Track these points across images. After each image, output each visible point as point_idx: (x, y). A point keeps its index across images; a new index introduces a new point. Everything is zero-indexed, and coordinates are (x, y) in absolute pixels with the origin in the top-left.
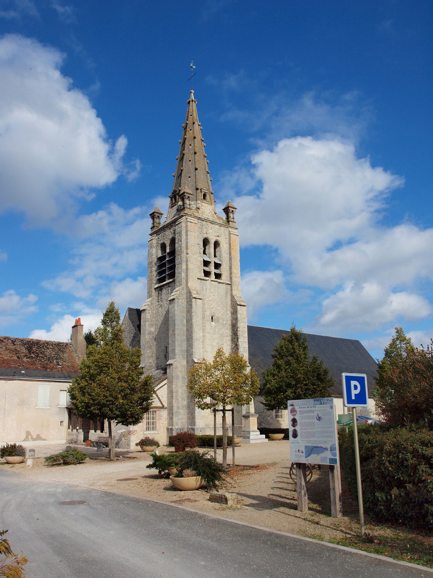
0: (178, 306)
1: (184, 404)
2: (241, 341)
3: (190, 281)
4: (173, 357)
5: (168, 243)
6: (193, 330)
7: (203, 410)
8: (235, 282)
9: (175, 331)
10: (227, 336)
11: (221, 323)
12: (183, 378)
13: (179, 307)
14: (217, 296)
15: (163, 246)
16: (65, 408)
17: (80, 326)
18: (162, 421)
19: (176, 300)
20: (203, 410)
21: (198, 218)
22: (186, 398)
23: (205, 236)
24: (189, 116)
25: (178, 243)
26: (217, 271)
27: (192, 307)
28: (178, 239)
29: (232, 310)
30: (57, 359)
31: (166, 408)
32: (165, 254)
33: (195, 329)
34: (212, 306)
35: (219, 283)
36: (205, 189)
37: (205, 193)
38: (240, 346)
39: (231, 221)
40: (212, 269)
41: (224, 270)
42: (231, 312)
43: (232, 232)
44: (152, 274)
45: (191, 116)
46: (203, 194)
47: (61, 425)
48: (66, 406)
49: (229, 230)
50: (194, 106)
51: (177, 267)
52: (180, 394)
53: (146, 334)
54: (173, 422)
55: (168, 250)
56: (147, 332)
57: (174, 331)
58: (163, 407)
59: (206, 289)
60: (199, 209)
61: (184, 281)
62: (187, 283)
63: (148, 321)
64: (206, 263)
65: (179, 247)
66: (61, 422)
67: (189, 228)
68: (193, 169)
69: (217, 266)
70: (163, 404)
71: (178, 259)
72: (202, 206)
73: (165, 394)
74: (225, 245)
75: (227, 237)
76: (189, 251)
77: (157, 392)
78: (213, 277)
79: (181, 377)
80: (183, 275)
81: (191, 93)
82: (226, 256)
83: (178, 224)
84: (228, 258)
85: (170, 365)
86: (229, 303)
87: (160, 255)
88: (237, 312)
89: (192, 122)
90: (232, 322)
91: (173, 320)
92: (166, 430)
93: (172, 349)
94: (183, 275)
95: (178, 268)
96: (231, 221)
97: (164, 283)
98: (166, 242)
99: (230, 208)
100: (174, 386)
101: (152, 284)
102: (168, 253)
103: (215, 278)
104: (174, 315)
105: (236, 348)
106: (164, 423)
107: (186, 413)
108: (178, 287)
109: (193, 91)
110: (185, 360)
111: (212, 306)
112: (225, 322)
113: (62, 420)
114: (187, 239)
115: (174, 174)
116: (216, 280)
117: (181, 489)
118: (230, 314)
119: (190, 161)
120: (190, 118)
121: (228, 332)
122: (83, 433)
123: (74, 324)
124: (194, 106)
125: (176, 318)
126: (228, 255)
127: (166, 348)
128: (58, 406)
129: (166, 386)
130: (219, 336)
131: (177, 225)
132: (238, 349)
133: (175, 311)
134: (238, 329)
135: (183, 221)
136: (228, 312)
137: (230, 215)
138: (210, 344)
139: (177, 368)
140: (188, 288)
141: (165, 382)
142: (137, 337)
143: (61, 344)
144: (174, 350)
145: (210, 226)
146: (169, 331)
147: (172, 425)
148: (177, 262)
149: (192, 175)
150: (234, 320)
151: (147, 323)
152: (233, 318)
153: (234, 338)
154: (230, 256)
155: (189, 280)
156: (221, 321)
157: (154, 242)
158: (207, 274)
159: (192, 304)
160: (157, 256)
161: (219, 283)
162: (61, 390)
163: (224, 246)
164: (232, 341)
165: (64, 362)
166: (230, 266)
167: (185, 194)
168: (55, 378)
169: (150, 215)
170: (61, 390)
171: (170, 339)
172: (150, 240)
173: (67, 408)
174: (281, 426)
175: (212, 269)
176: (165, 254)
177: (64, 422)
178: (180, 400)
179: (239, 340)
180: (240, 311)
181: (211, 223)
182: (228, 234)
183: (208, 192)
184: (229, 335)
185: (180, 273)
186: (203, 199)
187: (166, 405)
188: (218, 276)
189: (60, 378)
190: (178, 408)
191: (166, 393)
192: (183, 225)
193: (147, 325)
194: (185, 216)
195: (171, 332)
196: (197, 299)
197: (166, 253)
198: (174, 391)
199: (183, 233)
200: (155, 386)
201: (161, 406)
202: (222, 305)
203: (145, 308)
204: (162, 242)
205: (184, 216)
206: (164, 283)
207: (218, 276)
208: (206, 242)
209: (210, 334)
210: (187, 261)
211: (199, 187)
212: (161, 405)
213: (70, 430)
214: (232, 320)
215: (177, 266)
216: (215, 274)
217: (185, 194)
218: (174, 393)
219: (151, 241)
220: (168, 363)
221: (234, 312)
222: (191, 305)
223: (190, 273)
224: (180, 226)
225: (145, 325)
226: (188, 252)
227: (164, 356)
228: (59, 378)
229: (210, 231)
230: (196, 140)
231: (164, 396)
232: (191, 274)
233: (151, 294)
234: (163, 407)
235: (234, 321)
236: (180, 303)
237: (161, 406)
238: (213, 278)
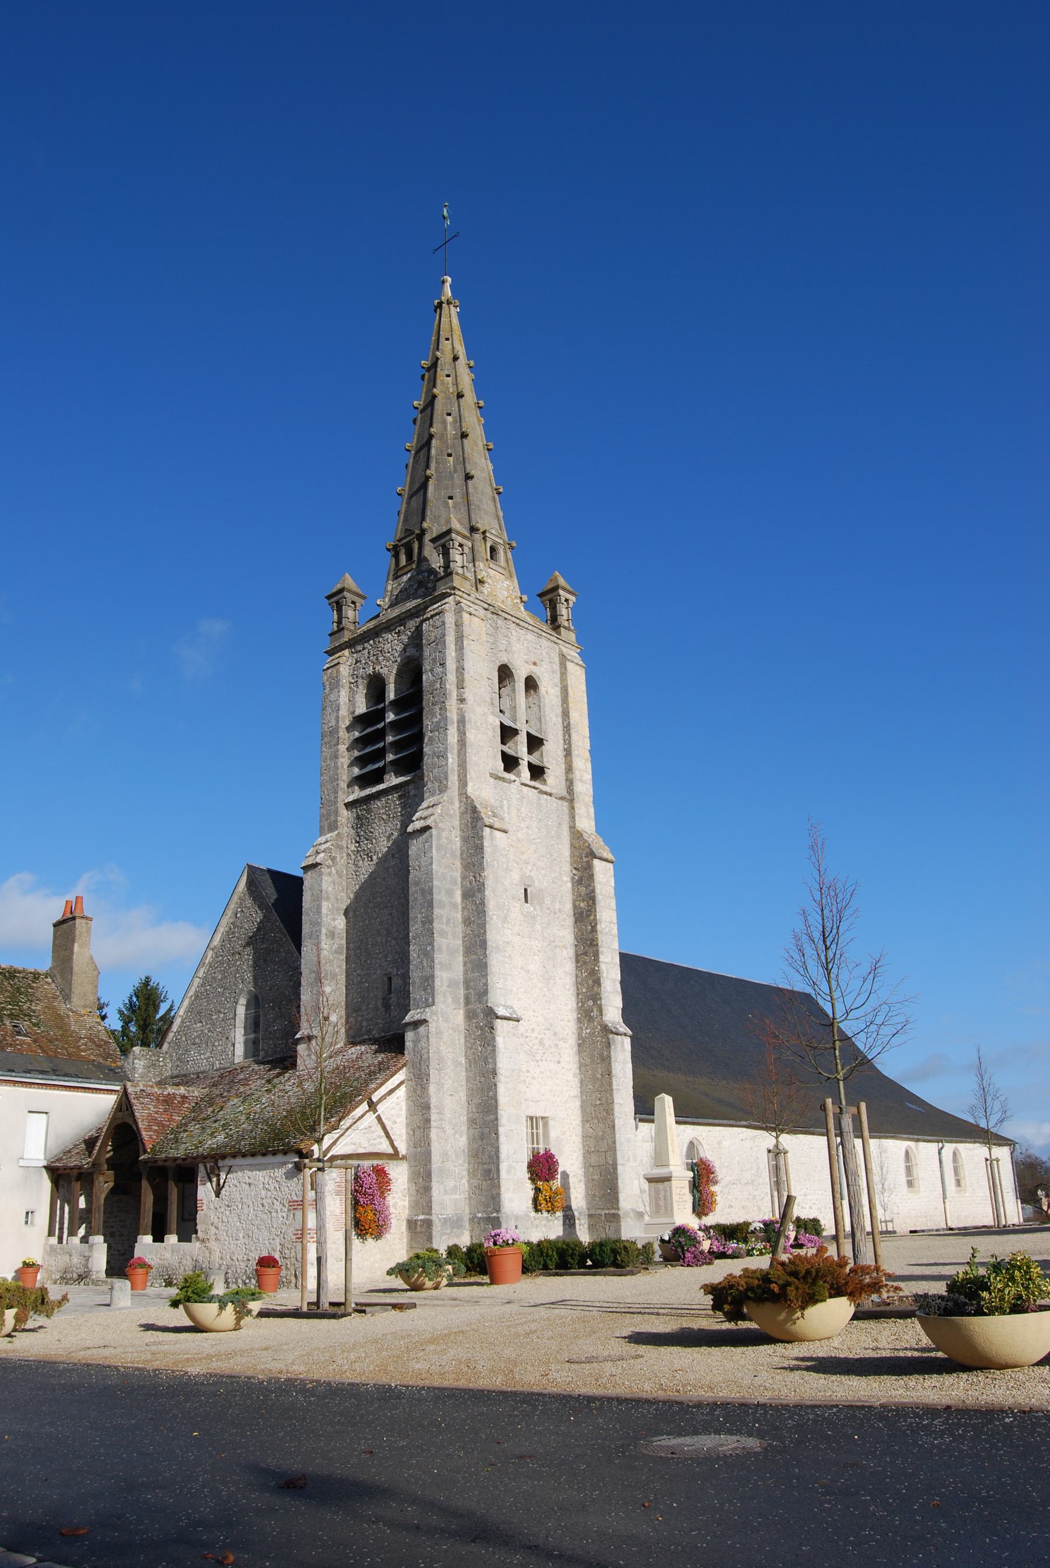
0: (439, 848)
1: (461, 1144)
2: (606, 960)
3: (471, 778)
4: (427, 1000)
5: (390, 672)
6: (487, 919)
7: (24, 1263)
8: (580, 793)
9: (432, 924)
10: (564, 947)
11: (548, 909)
12: (457, 1064)
13: (443, 853)
14: (537, 830)
15: (376, 686)
16: (44, 1171)
17: (84, 921)
18: (394, 1198)
19: (433, 830)
20: (24, 1263)
21: (486, 606)
22: (464, 1128)
23: (504, 659)
24: (442, 339)
25: (432, 670)
26: (534, 759)
27: (483, 853)
28: (434, 660)
29: (574, 872)
30: (12, 1016)
31: (404, 1158)
32: (382, 705)
33: (491, 919)
34: (524, 857)
35: (542, 792)
36: (493, 532)
37: (495, 542)
38: (605, 975)
39: (565, 628)
40: (520, 747)
41: (551, 755)
42: (573, 878)
43: (569, 655)
44: (336, 763)
45: (447, 339)
46: (489, 545)
47: (27, 1222)
48: (45, 1163)
49: (561, 650)
50: (451, 316)
51: (430, 738)
52: (448, 1114)
53: (323, 937)
54: (430, 1201)
55: (391, 695)
56: (324, 931)
57: (429, 921)
58: (395, 1156)
59: (509, 806)
60: (481, 582)
61: (453, 779)
62: (463, 783)
63: (328, 899)
64: (507, 733)
65: (434, 682)
66: (27, 1213)
67: (466, 630)
68: (459, 478)
69: (535, 743)
70: (396, 1144)
71: (434, 715)
72: (488, 575)
73: (399, 1116)
74: (552, 690)
75: (557, 667)
76: (468, 694)
77: (378, 1107)
78: (525, 773)
79: (449, 1062)
80: (452, 760)
81: (443, 282)
82: (554, 719)
83: (432, 616)
84: (560, 726)
85: (417, 1024)
86: (566, 851)
87: (361, 708)
88: (591, 877)
89: (449, 357)
90: (575, 907)
91: (423, 891)
92: (405, 1223)
93: (422, 977)
94: (450, 760)
95: (430, 738)
96: (565, 628)
97: (382, 787)
98: (384, 671)
99: (561, 592)
100: (432, 1089)
101: (336, 792)
102: (391, 702)
103: (531, 780)
104: (429, 874)
105: (590, 982)
106: (400, 1204)
107: (465, 1173)
108: (433, 795)
109: (449, 279)
110: (462, 1012)
111: (524, 857)
112: (557, 906)
113: (30, 1209)
114: (460, 659)
115: (399, 488)
116: (533, 783)
117: (1011, 1361)
118: (569, 885)
119: (450, 455)
120: (445, 345)
121: (565, 934)
122: (106, 1245)
123: (58, 917)
124: (451, 316)
125: (436, 883)
126: (560, 720)
127: (386, 979)
128: (22, 1163)
129: (403, 1088)
130: (546, 944)
131: (428, 619)
132: (599, 985)
133: (431, 864)
134: (599, 927)
135: (447, 608)
136: (565, 879)
137: (560, 611)
138: (522, 968)
139: (439, 1033)
140: (467, 797)
141: (400, 1076)
142: (278, 951)
143: (19, 973)
144: (429, 981)
145: (514, 633)
146: (411, 923)
147: (429, 1207)
148: (428, 723)
149: (458, 493)
150: (583, 901)
151: (325, 906)
152: (580, 895)
153: (585, 953)
154: (564, 720)
155: (468, 776)
156: (547, 901)
157: (345, 670)
158: (510, 763)
159: (482, 845)
160: (353, 712)
161: (542, 792)
162: (29, 1112)
163: (549, 689)
164: (577, 961)
165: (35, 1025)
166: (565, 750)
167: (454, 535)
168: (13, 1071)
169: (329, 597)
170: (29, 1112)
171: (412, 948)
172: (327, 666)
173: (47, 1168)
174: (618, 1230)
175: (520, 747)
176: (382, 705)
177: (36, 1214)
178: (449, 1131)
179: (602, 958)
180: (601, 876)
181: (518, 624)
182: (557, 660)
183: (502, 542)
184: (568, 946)
185: (443, 756)
186: (489, 558)
187: (403, 1150)
188: (537, 772)
189: (29, 1071)
190: (445, 1155)
191: (404, 1113)
192: (450, 619)
193: (324, 910)
194: (454, 594)
195: (415, 928)
196: (496, 829)
197: (384, 701)
198: (433, 1102)
199: (450, 639)
200: (376, 1090)
201: (391, 1151)
202: (548, 856)
203: (318, 860)
204: (370, 671)
205: (451, 595)
206: (382, 787)
207: (537, 772)
208: (505, 673)
209: (523, 937)
210: (462, 722)
211: (479, 525)
212: (390, 1147)
213: (54, 1240)
214: (574, 901)
215: (428, 735)
216: (531, 767)
217: (454, 535)
218: (433, 1111)
219: (334, 669)
220: (408, 1019)
221: (584, 877)
222: (479, 849)
223: (472, 757)
224: (439, 624)
225: (319, 911)
226: (465, 696)
227: (380, 1003)
228: (25, 1072)
229: (516, 647)
230: (462, 401)
231: (398, 1120)
232: (474, 758)
233: (336, 821)
234: (395, 1156)
235: (582, 905)
236: (444, 841)
237: (391, 1151)
238: (526, 779)
